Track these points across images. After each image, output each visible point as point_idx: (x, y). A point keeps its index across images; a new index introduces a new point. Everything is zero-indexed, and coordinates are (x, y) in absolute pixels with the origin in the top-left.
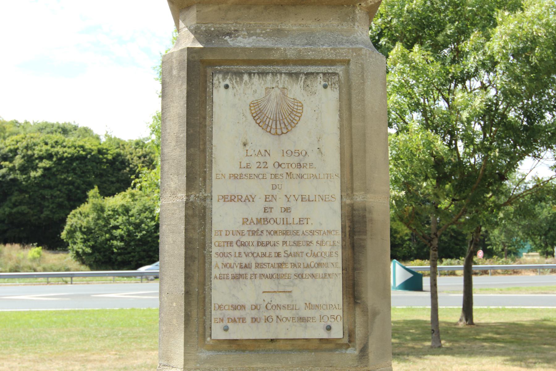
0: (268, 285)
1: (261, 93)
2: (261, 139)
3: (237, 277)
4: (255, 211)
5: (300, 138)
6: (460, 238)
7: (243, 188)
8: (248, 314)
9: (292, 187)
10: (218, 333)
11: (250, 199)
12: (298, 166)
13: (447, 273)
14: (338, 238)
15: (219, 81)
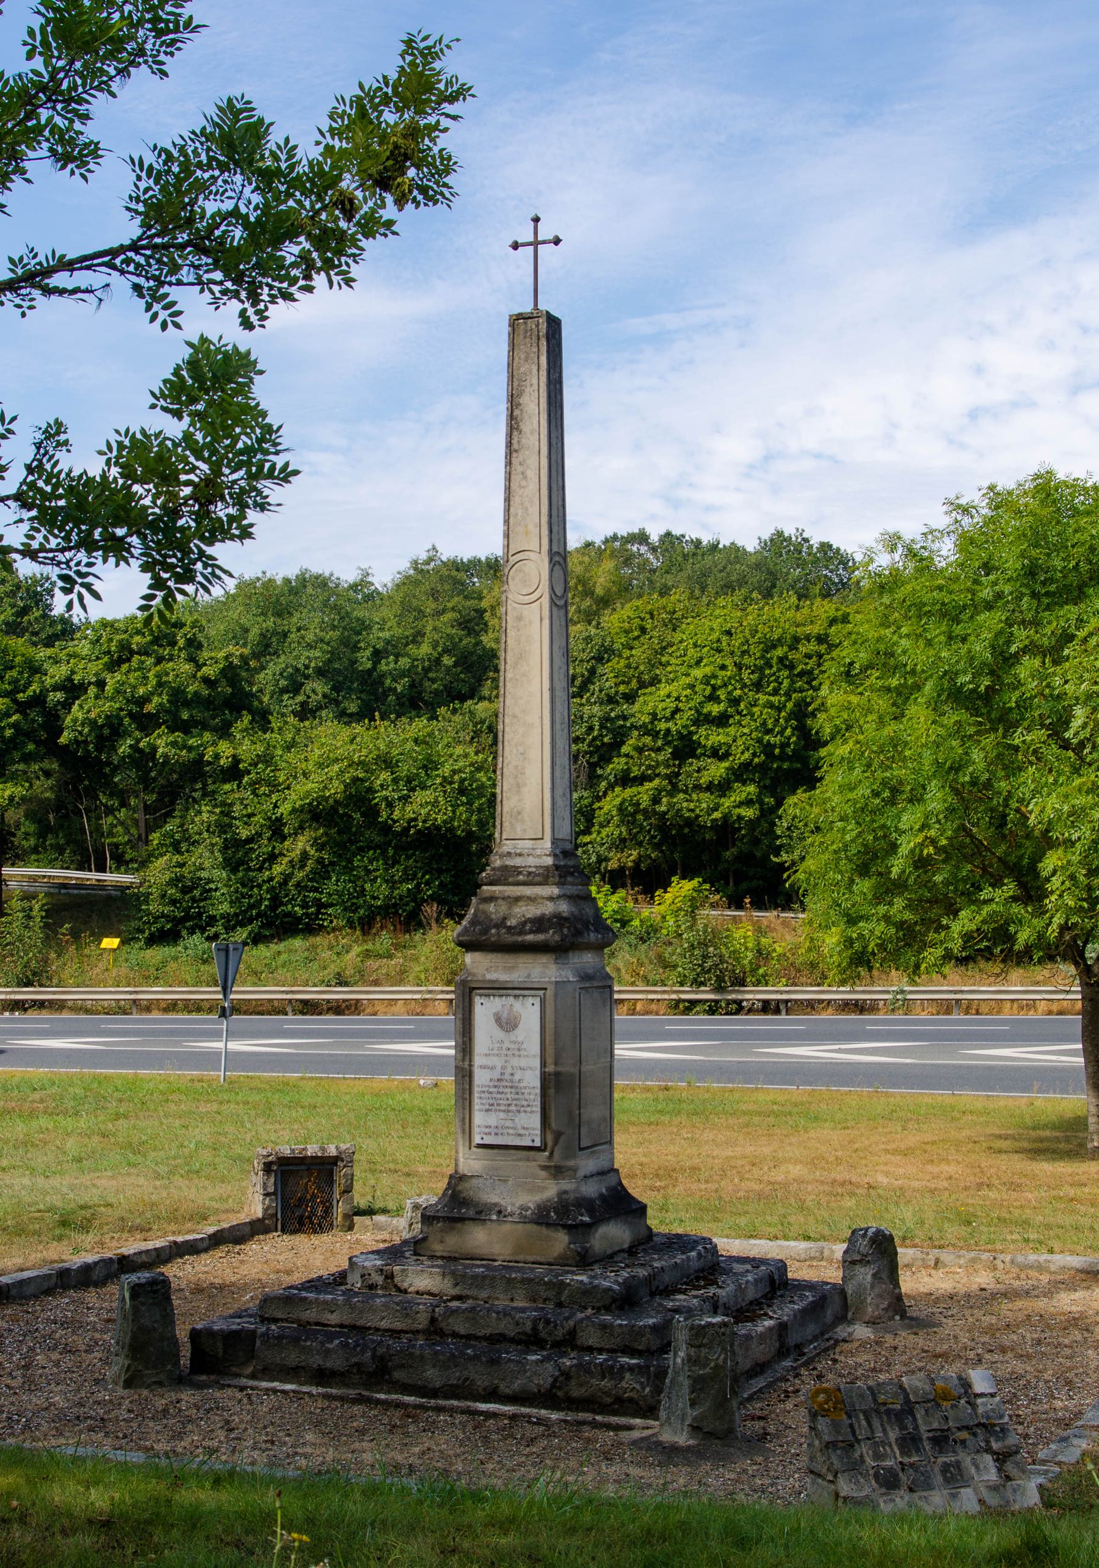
0: (502, 1115)
1: (499, 1008)
2: (500, 1034)
3: (487, 1110)
4: (496, 1075)
5: (520, 1034)
6: (222, 511)
7: (489, 1062)
8: (493, 1131)
9: (515, 1062)
10: (477, 1140)
11: (493, 1068)
12: (519, 1050)
13: (500, 902)
14: (538, 1091)
15: (477, 1000)
